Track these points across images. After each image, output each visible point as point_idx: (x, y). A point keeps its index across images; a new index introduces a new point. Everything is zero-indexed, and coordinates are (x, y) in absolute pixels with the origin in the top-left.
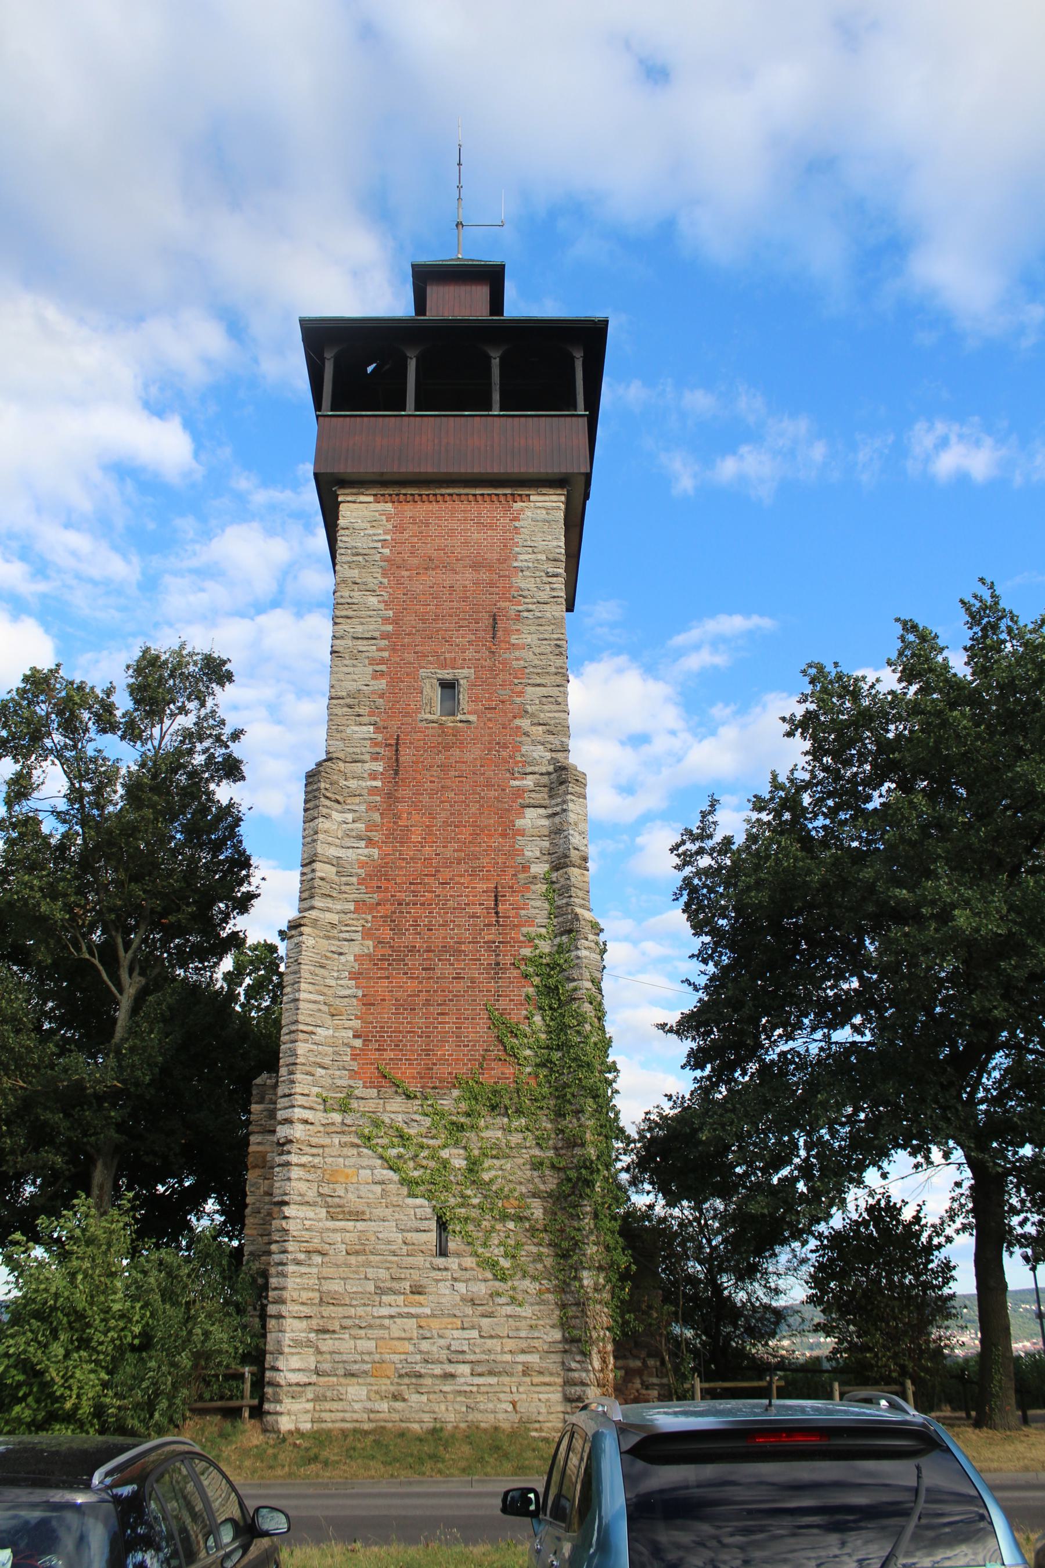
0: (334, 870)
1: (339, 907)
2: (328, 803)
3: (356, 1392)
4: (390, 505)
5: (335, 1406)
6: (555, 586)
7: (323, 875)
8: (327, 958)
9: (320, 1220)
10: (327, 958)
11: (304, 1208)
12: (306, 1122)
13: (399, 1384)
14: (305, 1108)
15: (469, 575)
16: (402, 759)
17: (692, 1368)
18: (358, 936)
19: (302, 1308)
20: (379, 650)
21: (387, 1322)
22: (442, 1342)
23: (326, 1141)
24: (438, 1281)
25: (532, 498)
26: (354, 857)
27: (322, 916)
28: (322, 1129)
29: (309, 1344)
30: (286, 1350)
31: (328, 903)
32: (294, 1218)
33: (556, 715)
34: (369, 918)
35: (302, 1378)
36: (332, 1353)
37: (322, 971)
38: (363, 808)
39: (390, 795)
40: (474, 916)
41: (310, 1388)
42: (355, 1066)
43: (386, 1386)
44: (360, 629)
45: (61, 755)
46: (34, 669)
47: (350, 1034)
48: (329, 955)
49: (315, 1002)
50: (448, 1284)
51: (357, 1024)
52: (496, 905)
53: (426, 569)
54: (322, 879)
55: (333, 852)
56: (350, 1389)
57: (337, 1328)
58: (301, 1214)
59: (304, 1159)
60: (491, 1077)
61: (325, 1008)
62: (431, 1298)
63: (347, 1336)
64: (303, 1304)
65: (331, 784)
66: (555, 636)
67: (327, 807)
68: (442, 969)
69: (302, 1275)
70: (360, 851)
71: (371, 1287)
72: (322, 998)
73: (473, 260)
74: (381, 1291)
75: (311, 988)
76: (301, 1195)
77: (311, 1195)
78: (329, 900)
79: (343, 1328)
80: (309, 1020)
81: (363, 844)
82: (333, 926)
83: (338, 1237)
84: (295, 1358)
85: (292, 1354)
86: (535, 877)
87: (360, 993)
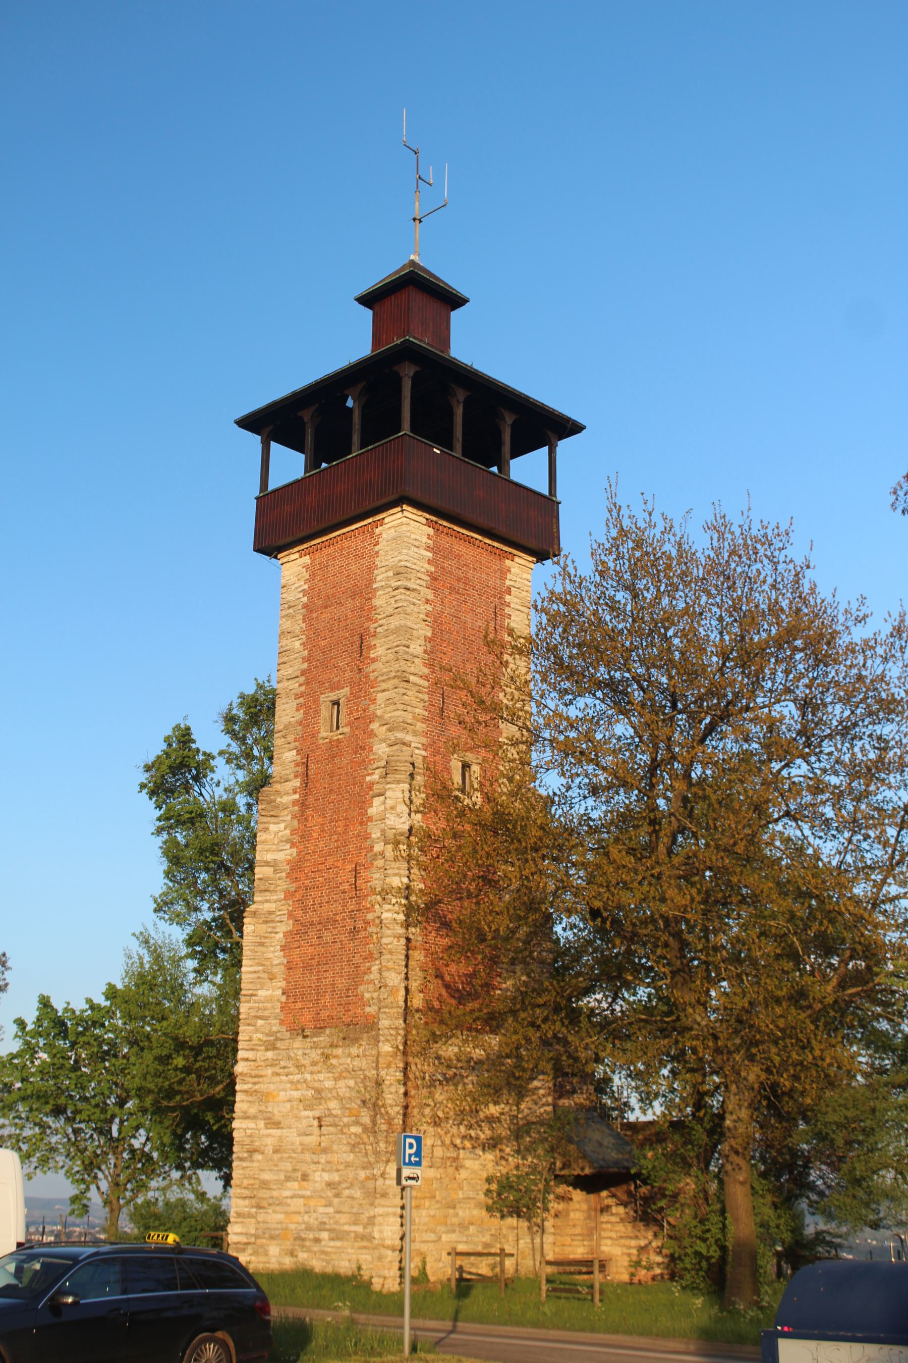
0: (272, 869)
1: (275, 897)
3: (274, 1250)
4: (431, 529)
6: (396, 598)
7: (261, 876)
8: (265, 938)
10: (265, 938)
11: (246, 1121)
12: (247, 1060)
14: (247, 1050)
15: (349, 603)
16: (309, 773)
18: (285, 918)
19: (243, 1191)
20: (300, 685)
22: (314, 1215)
26: (284, 857)
27: (261, 907)
28: (262, 1064)
29: (250, 1216)
31: (268, 896)
32: (238, 1129)
33: (393, 714)
34: (291, 903)
35: (243, 1239)
38: (289, 818)
39: (303, 804)
40: (344, 892)
43: (288, 1245)
44: (290, 671)
45: (597, 747)
47: (280, 992)
48: (267, 935)
49: (255, 972)
50: (319, 1173)
52: (356, 881)
53: (326, 608)
55: (269, 857)
57: (266, 1205)
58: (244, 1126)
60: (349, 1016)
63: (270, 1211)
64: (245, 1188)
66: (395, 644)
67: (265, 823)
68: (327, 936)
69: (244, 1168)
70: (286, 852)
71: (282, 1177)
72: (261, 968)
73: (447, 284)
75: (250, 963)
77: (253, 1111)
78: (267, 894)
79: (269, 1205)
80: (250, 986)
81: (288, 846)
82: (270, 913)
84: (237, 1225)
85: (237, 1223)
86: (376, 855)
87: (285, 962)
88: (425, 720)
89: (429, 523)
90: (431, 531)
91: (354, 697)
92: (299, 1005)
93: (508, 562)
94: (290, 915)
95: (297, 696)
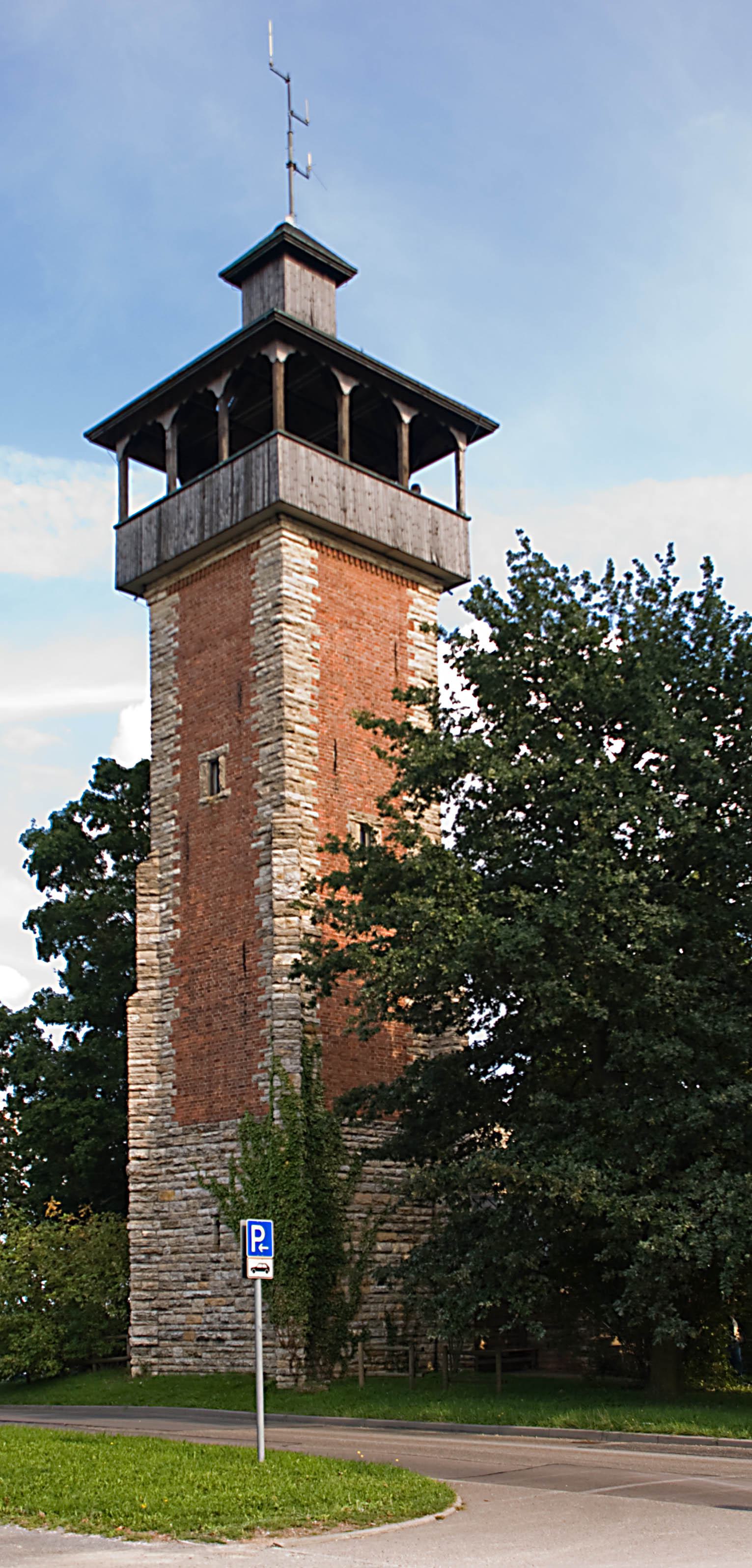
2: (144, 899)
5: (167, 1360)
9: (157, 1230)
13: (197, 1346)
17: (689, 1337)
21: (190, 1301)
23: (157, 1171)
24: (215, 1270)
25: (262, 543)
30: (132, 1322)
36: (166, 1324)
37: (147, 1040)
38: (170, 895)
41: (153, 1349)
42: (173, 1110)
46: (28, 840)
47: (170, 1085)
49: (142, 1065)
51: (174, 1077)
54: (143, 965)
56: (175, 1349)
59: (139, 1187)
61: (154, 1068)
62: (211, 1283)
64: (145, 1290)
65: (147, 881)
69: (142, 1270)
74: (188, 1280)
75: (138, 1055)
76: (137, 1213)
81: (171, 927)
83: (166, 1241)
88: (316, 776)
89: (313, 543)
90: (315, 553)
91: (233, 756)
92: (191, 1098)
93: (410, 591)
94: (177, 1003)
95: (174, 757)
